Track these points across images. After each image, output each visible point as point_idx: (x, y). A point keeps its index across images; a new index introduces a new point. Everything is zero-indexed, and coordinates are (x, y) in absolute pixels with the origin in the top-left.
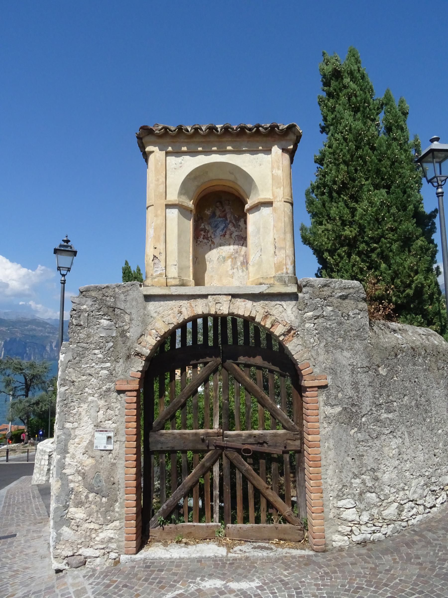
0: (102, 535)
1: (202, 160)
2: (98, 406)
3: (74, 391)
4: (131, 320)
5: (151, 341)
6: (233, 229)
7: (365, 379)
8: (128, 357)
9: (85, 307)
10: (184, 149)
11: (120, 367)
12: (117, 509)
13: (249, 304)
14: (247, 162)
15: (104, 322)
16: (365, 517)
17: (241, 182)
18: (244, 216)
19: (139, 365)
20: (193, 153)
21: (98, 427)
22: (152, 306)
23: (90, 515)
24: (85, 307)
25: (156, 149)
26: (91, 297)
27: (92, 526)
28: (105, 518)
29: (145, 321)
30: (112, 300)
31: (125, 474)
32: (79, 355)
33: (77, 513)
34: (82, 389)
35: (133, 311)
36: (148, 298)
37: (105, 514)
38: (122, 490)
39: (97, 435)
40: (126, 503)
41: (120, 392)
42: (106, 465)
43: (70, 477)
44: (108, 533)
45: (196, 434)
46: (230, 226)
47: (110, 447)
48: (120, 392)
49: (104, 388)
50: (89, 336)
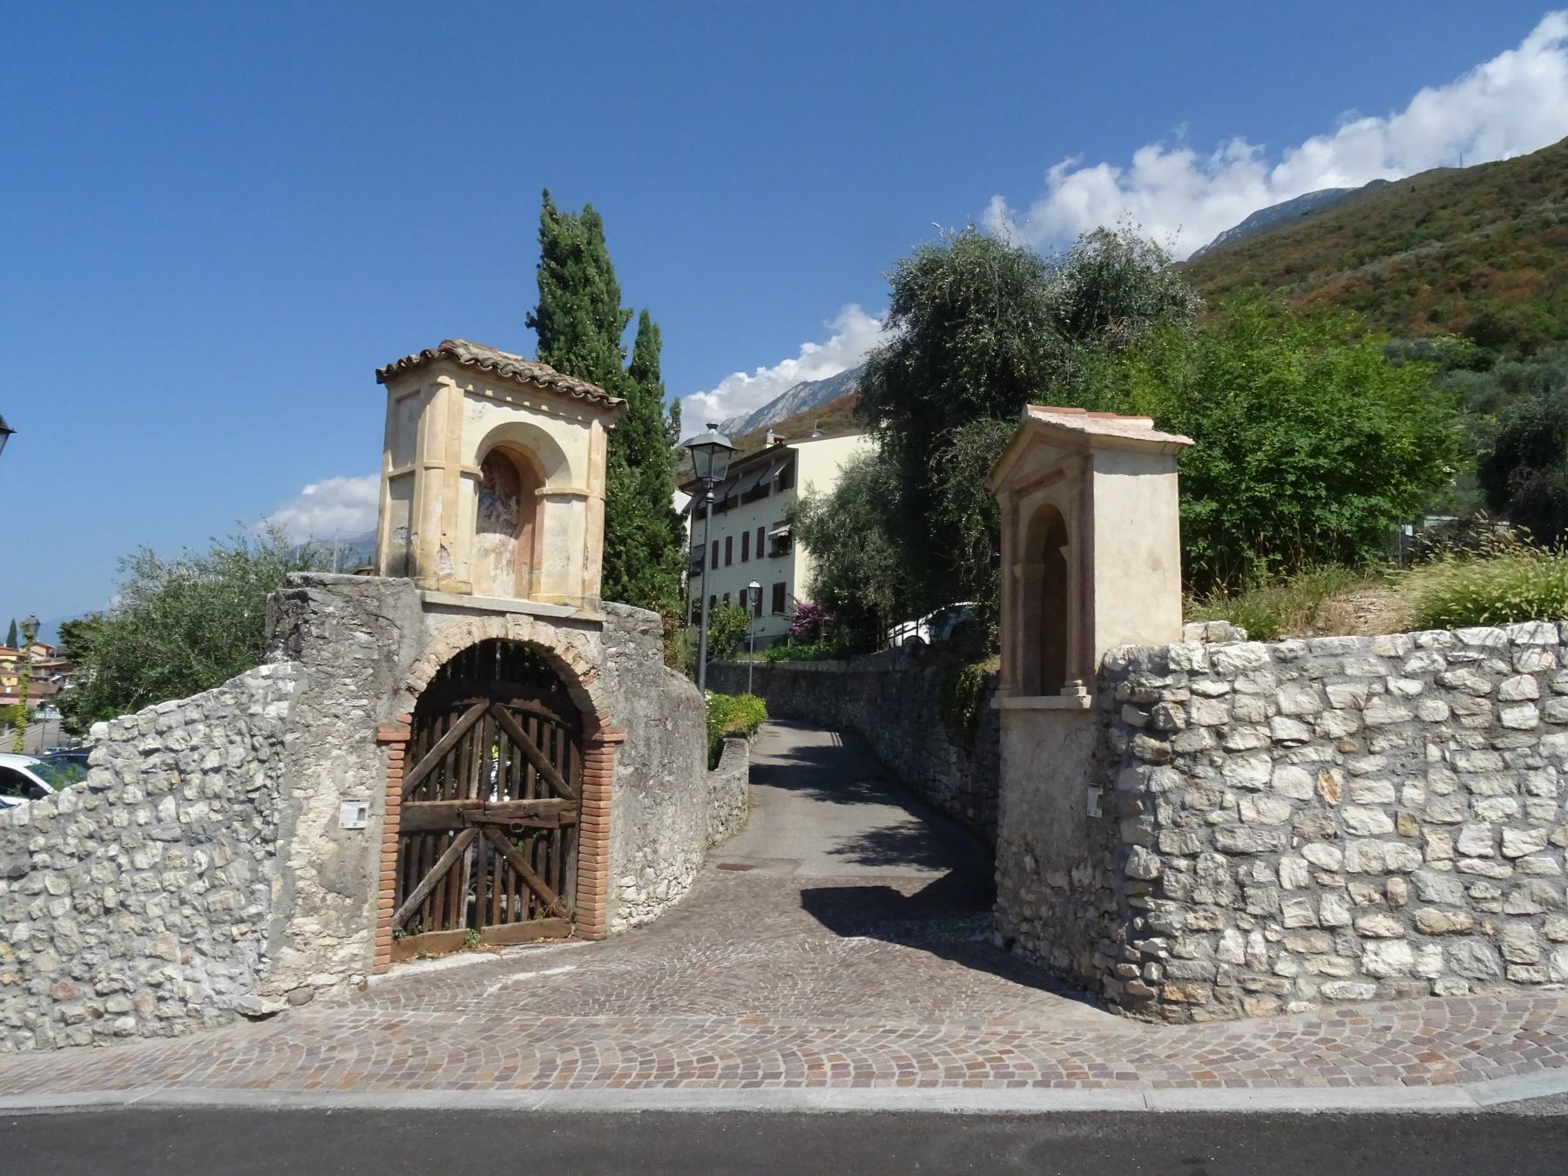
0: (342, 953)
1: (507, 415)
2: (346, 764)
3: (310, 740)
4: (401, 637)
5: (429, 670)
6: (501, 509)
7: (656, 734)
8: (396, 692)
9: (331, 609)
10: (489, 393)
11: (382, 706)
12: (365, 914)
13: (551, 629)
14: (558, 430)
15: (362, 637)
16: (643, 897)
17: (543, 456)
18: (535, 501)
19: (410, 704)
20: (498, 401)
21: (345, 795)
22: (432, 619)
23: (326, 925)
24: (331, 609)
25: (452, 382)
26: (340, 594)
27: (329, 941)
28: (347, 926)
29: (421, 642)
30: (376, 603)
31: (381, 860)
32: (319, 684)
33: (309, 925)
34: (321, 738)
35: (406, 624)
36: (428, 607)
37: (347, 922)
38: (375, 885)
39: (345, 806)
40: (379, 901)
41: (380, 743)
42: (353, 852)
43: (298, 872)
44: (351, 948)
45: (451, 806)
46: (498, 503)
47: (361, 824)
48: (380, 743)
49: (357, 737)
50: (336, 656)
